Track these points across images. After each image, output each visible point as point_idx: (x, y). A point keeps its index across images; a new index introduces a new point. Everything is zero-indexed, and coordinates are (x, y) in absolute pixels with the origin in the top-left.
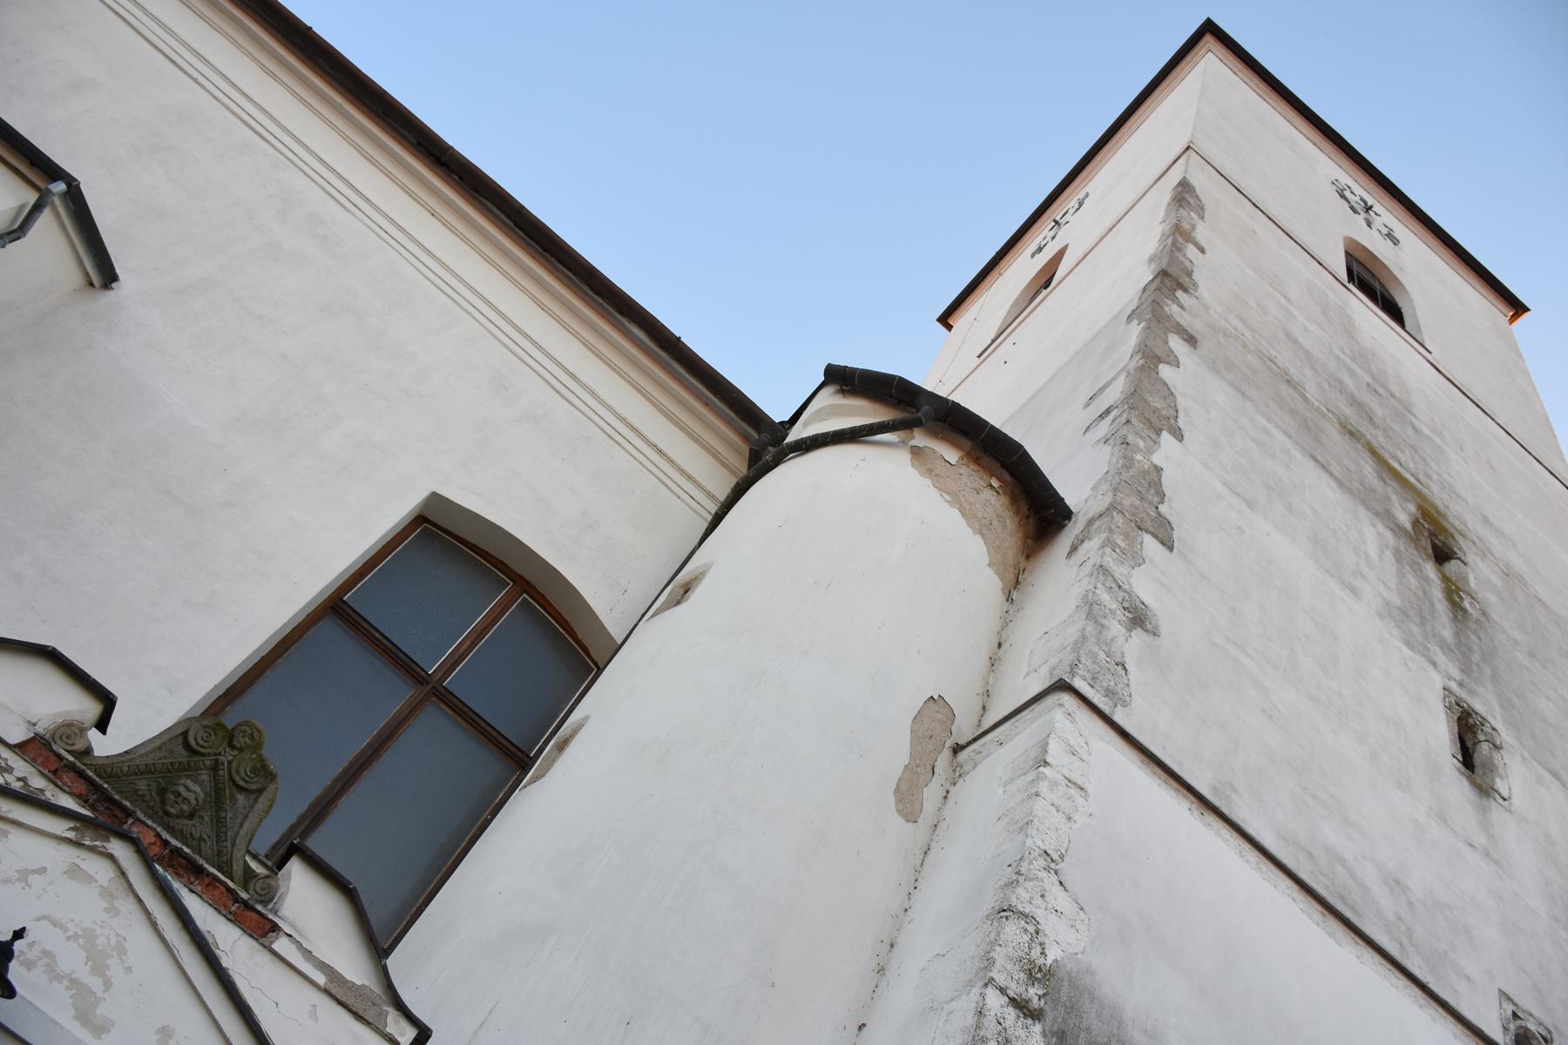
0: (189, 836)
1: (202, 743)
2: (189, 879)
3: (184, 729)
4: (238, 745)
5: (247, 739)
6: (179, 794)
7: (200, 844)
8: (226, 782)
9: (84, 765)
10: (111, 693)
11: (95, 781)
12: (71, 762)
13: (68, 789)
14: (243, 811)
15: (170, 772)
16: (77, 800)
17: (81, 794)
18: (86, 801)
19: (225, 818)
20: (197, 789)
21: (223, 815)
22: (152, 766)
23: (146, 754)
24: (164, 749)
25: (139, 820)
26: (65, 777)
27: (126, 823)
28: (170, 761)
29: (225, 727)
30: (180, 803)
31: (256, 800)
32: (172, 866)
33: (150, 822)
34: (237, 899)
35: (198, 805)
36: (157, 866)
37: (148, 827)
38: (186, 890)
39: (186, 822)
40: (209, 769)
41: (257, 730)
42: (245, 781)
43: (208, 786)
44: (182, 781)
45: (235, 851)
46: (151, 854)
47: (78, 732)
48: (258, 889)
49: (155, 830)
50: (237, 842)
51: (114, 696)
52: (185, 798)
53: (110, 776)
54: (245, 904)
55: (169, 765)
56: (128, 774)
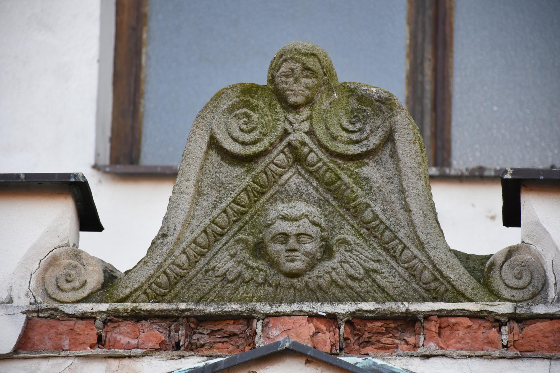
0: (350, 282)
1: (248, 138)
2: (407, 343)
3: (207, 140)
4: (300, 99)
5: (304, 80)
6: (286, 236)
7: (374, 281)
8: (331, 165)
9: (123, 300)
10: (68, 175)
11: (161, 311)
12: (108, 312)
13: (139, 351)
14: (390, 187)
15: (243, 214)
16: (164, 353)
17: (162, 343)
18: (177, 346)
19: (376, 217)
20: (300, 208)
21: (368, 215)
22: (214, 227)
23: (191, 216)
24: (205, 190)
25: (268, 316)
26: (119, 337)
27: (255, 333)
28: (229, 199)
29: (258, 87)
30: (297, 247)
31: (394, 154)
32: (368, 343)
33: (285, 308)
34: (498, 321)
35: (322, 230)
36: (351, 360)
37: (289, 315)
38: (417, 361)
39: (328, 265)
40: (291, 167)
41: (307, 55)
42: (357, 142)
43: (312, 191)
44: (272, 214)
45: (431, 254)
46: (327, 349)
47: (74, 262)
48: (513, 282)
49: (300, 313)
50: (423, 237)
51: (76, 175)
52: (298, 235)
53: (172, 285)
54: (514, 318)
55: (233, 205)
56: (192, 264)
